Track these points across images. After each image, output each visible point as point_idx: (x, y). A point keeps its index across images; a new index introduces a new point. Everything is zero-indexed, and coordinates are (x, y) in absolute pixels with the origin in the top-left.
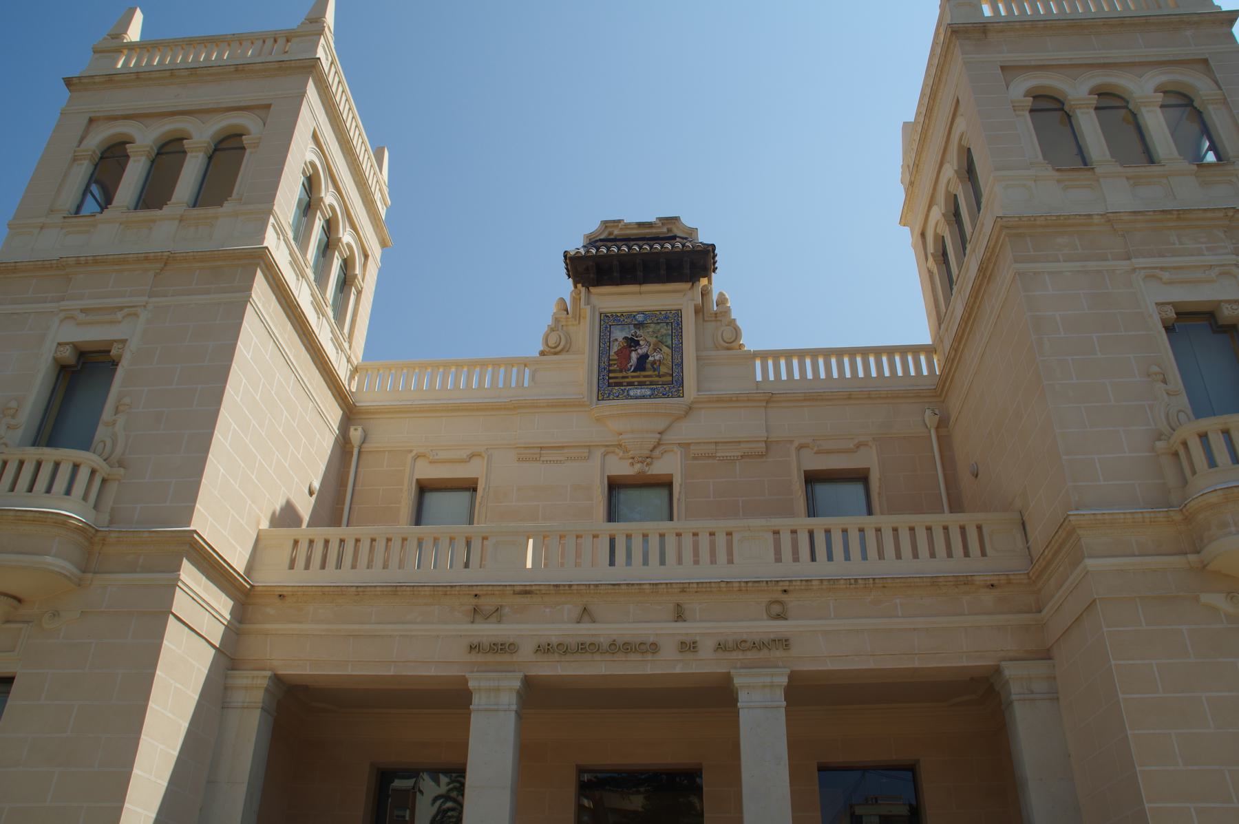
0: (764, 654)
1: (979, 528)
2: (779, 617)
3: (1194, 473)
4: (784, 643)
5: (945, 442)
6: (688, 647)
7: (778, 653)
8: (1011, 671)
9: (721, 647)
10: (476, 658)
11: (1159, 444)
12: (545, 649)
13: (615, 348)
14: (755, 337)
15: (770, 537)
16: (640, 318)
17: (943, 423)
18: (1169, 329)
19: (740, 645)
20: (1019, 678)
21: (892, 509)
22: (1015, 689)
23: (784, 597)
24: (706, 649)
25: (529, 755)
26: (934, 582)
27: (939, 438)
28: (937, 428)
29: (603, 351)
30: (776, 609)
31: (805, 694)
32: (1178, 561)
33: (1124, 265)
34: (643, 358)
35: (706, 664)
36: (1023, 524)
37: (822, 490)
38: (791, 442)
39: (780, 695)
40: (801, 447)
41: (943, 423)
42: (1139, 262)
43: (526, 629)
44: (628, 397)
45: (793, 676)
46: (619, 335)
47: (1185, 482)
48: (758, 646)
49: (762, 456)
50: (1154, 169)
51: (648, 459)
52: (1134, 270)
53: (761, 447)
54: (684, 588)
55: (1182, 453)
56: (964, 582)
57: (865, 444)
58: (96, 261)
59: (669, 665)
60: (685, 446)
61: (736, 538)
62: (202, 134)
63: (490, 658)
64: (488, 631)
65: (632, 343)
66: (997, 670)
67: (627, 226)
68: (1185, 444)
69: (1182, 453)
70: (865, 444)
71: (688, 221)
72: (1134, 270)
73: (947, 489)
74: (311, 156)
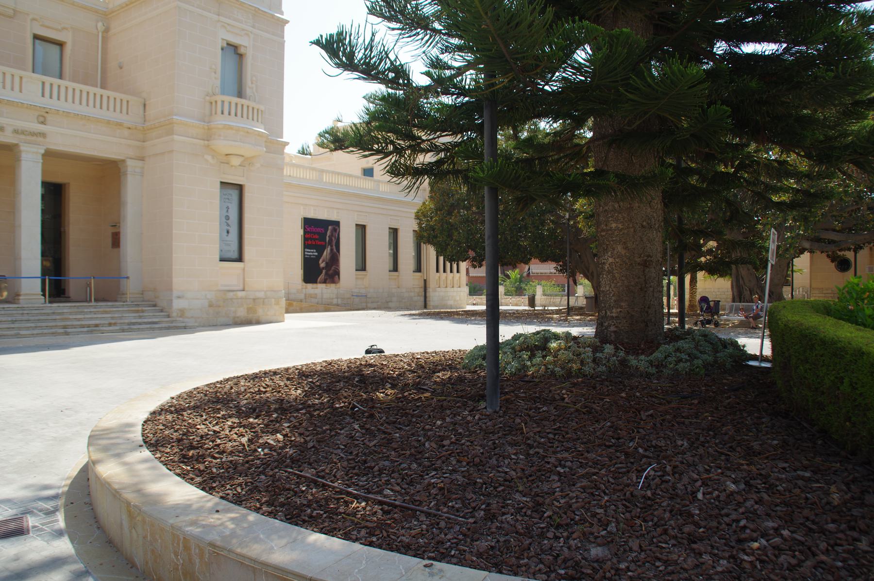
0: (34, 138)
1: (128, 102)
2: (43, 123)
4: (43, 135)
5: (105, 40)
7: (40, 139)
8: (130, 163)
9: (16, 131)
11: (208, 98)
17: (107, 30)
18: (222, 49)
19: (23, 133)
20: (132, 166)
22: (129, 169)
23: (46, 115)
26: (109, 122)
27: (103, 37)
28: (103, 32)
30: (42, 119)
31: (49, 155)
32: (202, 142)
33: (215, 17)
36: (145, 105)
37: (235, 194)
38: (28, 14)
39: (40, 157)
40: (33, 19)
41: (107, 30)
42: (222, 19)
47: (211, 115)
48: (33, 134)
49: (10, 17)
52: (219, 21)
53: (11, 12)
55: (214, 104)
56: (119, 125)
57: (66, 29)
61: (24, 80)
66: (123, 161)
68: (216, 102)
69: (214, 104)
70: (66, 29)
72: (219, 21)
73: (102, 63)
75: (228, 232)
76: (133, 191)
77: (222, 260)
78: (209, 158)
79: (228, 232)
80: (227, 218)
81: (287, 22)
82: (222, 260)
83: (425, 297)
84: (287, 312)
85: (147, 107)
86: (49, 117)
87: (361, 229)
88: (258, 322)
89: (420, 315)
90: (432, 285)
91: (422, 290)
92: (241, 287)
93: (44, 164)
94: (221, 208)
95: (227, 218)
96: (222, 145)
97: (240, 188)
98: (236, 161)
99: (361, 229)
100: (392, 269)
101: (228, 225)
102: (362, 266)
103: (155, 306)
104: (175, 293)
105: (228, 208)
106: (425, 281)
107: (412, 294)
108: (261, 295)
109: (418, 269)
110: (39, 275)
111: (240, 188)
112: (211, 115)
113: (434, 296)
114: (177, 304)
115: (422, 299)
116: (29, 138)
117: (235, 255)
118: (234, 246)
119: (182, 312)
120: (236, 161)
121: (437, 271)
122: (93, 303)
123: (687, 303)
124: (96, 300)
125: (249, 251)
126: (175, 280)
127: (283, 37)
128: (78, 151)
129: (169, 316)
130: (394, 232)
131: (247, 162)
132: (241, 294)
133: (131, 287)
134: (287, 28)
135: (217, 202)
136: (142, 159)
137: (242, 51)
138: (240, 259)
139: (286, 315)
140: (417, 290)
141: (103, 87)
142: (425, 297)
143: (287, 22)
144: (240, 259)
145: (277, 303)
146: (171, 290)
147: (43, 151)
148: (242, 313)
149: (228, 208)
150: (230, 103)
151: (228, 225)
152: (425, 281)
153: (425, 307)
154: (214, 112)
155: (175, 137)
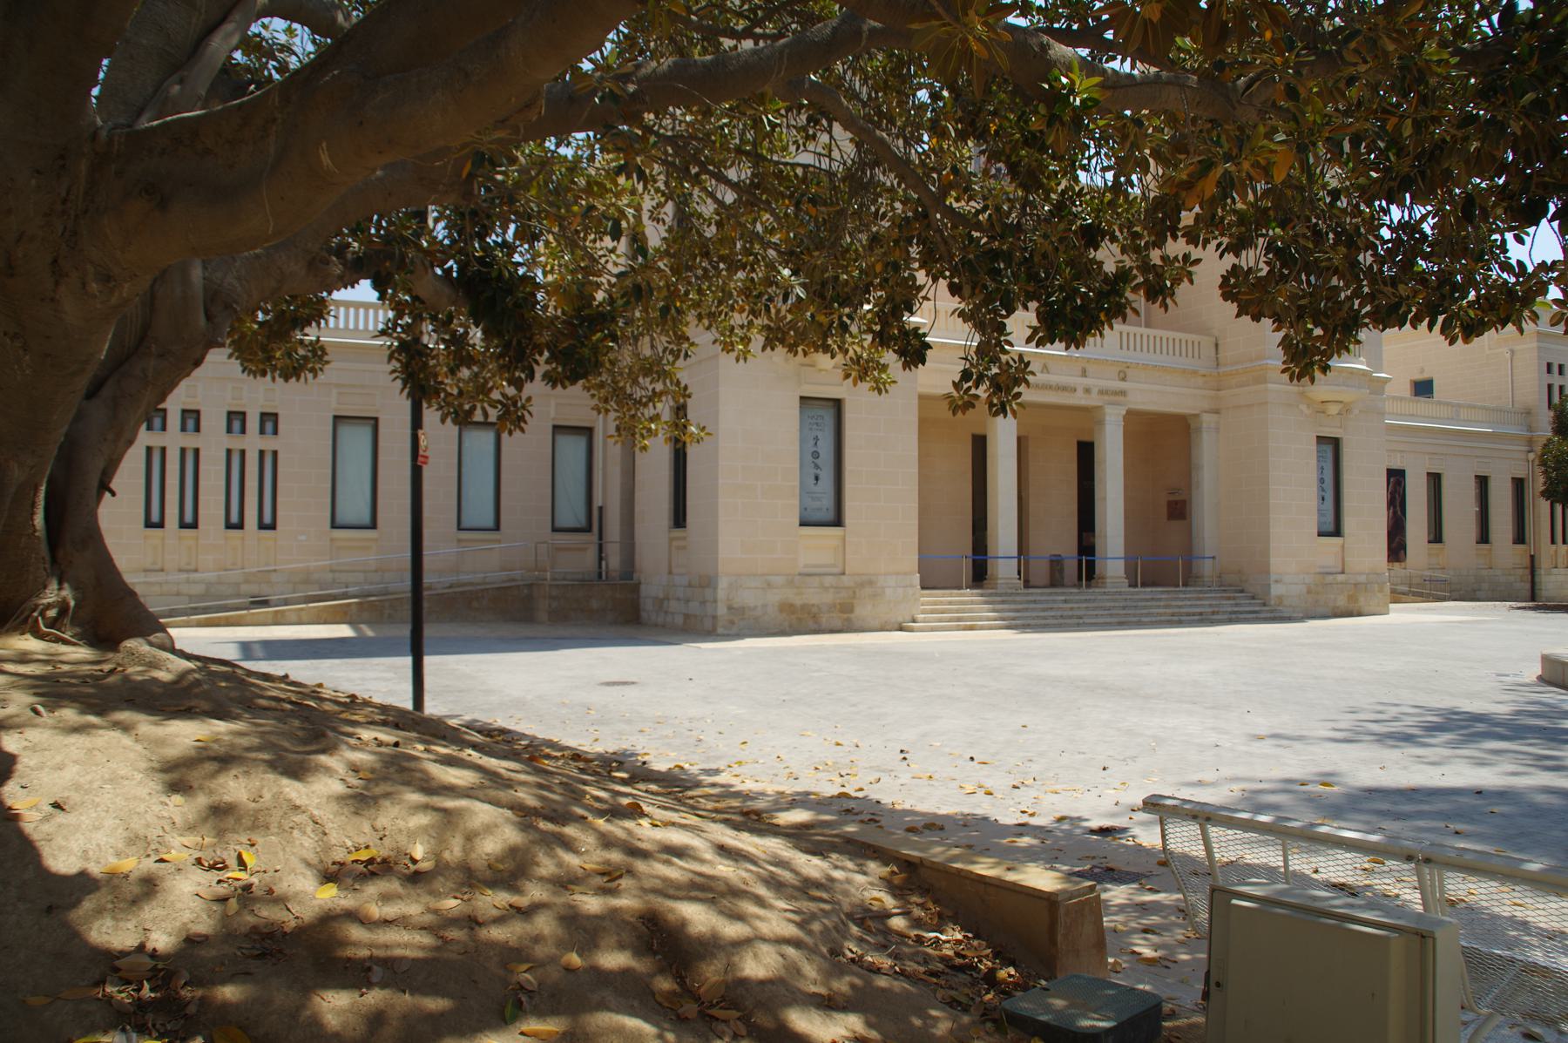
2: (1124, 379)
4: (1123, 393)
6: (1087, 391)
7: (1121, 398)
9: (1101, 392)
20: (1208, 420)
24: (1095, 391)
26: (1184, 371)
37: (1329, 449)
48: (1116, 393)
59: (1079, 399)
66: (1196, 416)
75: (817, 478)
76: (1210, 454)
77: (802, 524)
78: (1303, 407)
79: (817, 478)
80: (816, 455)
82: (1320, 534)
86: (1129, 372)
87: (1435, 480)
88: (1360, 615)
89: (1530, 608)
90: (1544, 563)
91: (1528, 572)
94: (802, 441)
95: (816, 455)
99: (1435, 480)
101: (817, 467)
102: (1436, 536)
103: (1242, 591)
104: (1273, 577)
105: (816, 439)
106: (1532, 557)
107: (1512, 579)
108: (1362, 579)
109: (1520, 538)
114: (1276, 590)
115: (1528, 586)
116: (1112, 398)
117: (830, 516)
118: (828, 502)
119: (1280, 598)
120: (1333, 409)
121: (1553, 542)
123: (344, 631)
124: (1143, 585)
125: (1349, 523)
126: (1272, 560)
130: (1483, 482)
131: (1346, 409)
132: (1340, 578)
133: (1207, 568)
135: (1314, 461)
136: (1217, 412)
138: (838, 522)
139: (1392, 606)
140: (1520, 572)
141: (1148, 325)
144: (838, 522)
145: (1381, 591)
146: (1268, 572)
148: (1342, 602)
149: (816, 439)
151: (817, 467)
152: (1532, 557)
153: (1533, 600)
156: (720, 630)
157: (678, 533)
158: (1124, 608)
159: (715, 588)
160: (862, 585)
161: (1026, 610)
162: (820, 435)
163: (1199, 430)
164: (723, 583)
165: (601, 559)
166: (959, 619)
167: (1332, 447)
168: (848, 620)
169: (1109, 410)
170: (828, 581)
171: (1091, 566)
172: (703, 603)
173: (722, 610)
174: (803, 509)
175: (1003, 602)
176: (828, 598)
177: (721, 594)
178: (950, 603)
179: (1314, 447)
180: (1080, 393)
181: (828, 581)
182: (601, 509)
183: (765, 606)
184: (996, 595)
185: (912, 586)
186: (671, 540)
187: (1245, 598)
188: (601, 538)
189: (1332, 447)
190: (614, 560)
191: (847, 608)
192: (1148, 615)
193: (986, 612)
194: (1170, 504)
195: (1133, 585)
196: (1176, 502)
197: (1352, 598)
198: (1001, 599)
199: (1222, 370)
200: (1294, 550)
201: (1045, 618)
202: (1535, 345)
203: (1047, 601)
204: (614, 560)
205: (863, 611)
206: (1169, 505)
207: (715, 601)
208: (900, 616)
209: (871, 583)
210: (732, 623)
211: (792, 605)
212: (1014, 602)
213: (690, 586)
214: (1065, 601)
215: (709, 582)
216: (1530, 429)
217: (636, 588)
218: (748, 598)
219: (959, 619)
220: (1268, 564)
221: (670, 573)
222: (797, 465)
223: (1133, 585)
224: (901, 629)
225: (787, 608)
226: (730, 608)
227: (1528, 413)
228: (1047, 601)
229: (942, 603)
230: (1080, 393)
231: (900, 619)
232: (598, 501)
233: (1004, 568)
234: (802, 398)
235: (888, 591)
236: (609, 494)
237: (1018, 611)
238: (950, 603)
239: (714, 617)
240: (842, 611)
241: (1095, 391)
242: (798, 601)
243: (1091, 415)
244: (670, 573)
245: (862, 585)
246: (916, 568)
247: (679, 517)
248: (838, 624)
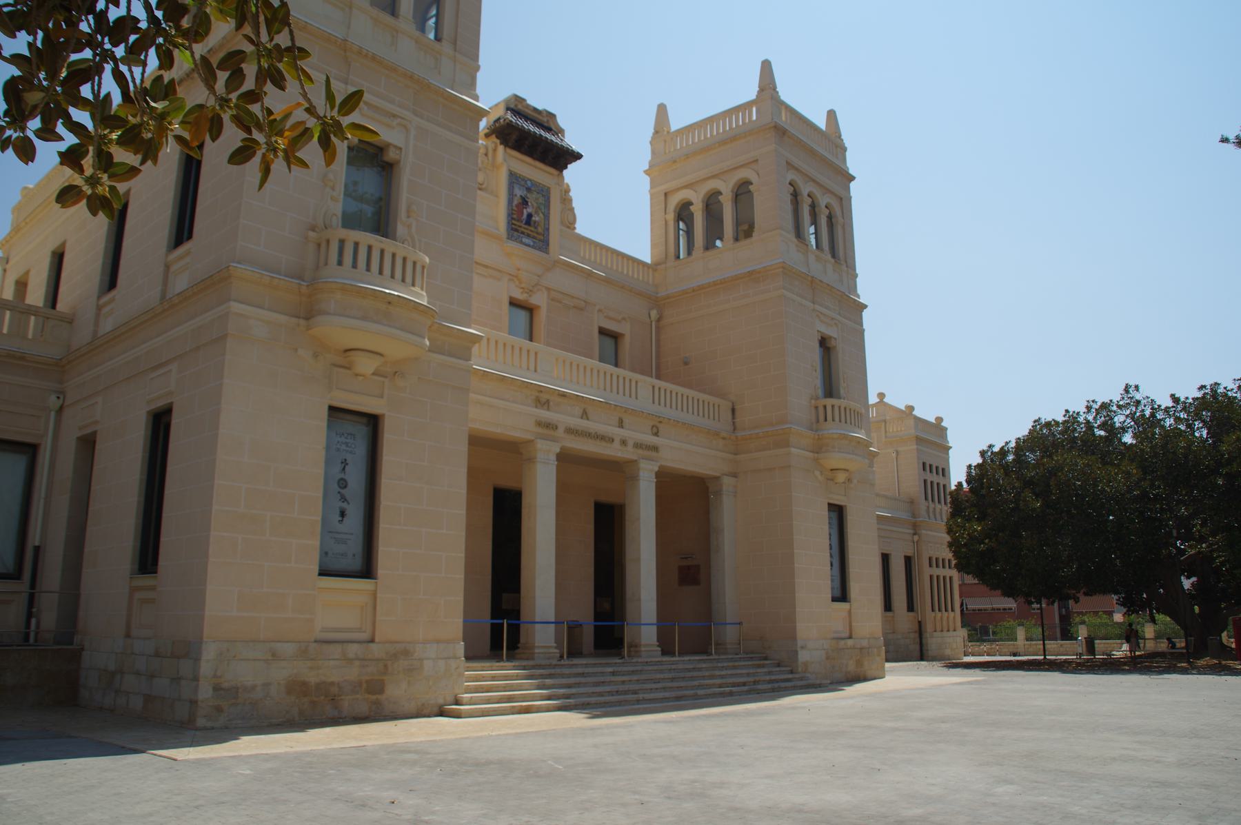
2: (656, 434)
3: (326, 264)
4: (655, 449)
6: (624, 442)
9: (638, 446)
10: (540, 430)
11: (311, 234)
12: (570, 431)
13: (515, 202)
14: (581, 228)
15: (539, 369)
16: (529, 183)
20: (727, 482)
21: (633, 370)
22: (724, 488)
24: (631, 443)
25: (563, 489)
29: (510, 201)
32: (811, 454)
34: (530, 216)
35: (627, 453)
36: (733, 411)
37: (361, 431)
42: (817, 307)
43: (565, 418)
44: (521, 242)
45: (661, 467)
46: (519, 192)
47: (317, 267)
50: (388, 18)
51: (531, 292)
54: (626, 410)
55: (324, 245)
58: (374, 58)
60: (548, 289)
62: (726, 188)
63: (545, 431)
64: (544, 414)
65: (524, 202)
66: (717, 478)
67: (528, 106)
68: (328, 241)
69: (324, 245)
71: (562, 121)
74: (810, 200)
75: (343, 514)
76: (730, 518)
77: (323, 573)
78: (817, 473)
79: (343, 514)
80: (343, 484)
81: (866, 307)
83: (921, 644)
84: (887, 661)
85: (737, 413)
90: (929, 627)
92: (847, 635)
93: (471, 455)
94: (328, 462)
95: (343, 484)
96: (834, 460)
97: (373, 422)
98: (367, 366)
100: (838, 594)
104: (800, 643)
108: (865, 643)
109: (911, 608)
110: (655, 621)
111: (373, 422)
112: (317, 267)
113: (933, 642)
114: (803, 656)
115: (917, 647)
119: (806, 664)
120: (841, 477)
122: (715, 657)
124: (680, 654)
127: (861, 325)
128: (499, 431)
129: (792, 672)
131: (392, 372)
132: (850, 642)
133: (730, 634)
134: (865, 313)
136: (735, 475)
137: (391, 155)
138: (367, 571)
139: (888, 665)
140: (912, 635)
142: (921, 644)
143: (866, 307)
144: (367, 571)
147: (558, 450)
148: (851, 667)
150: (370, 248)
154: (822, 418)
155: (793, 450)
156: (201, 722)
157: (146, 580)
158: (673, 679)
159: (197, 660)
160: (395, 656)
161: (578, 685)
162: (349, 457)
163: (719, 493)
164: (209, 653)
165: (30, 615)
166: (510, 699)
167: (838, 513)
168: (378, 703)
169: (643, 464)
170: (353, 650)
171: (515, 631)
172: (176, 680)
173: (205, 692)
174: (324, 554)
175: (550, 676)
176: (352, 673)
177: (206, 668)
178: (494, 678)
179: (826, 513)
180: (617, 444)
181: (353, 650)
182: (37, 549)
183: (267, 685)
184: (533, 667)
185: (456, 658)
186: (133, 590)
187: (771, 669)
188: (33, 586)
189: (838, 513)
190: (49, 617)
191: (376, 687)
192: (700, 687)
193: (529, 689)
194: (681, 569)
195: (665, 652)
196: (689, 568)
197: (859, 663)
198: (542, 672)
199: (740, 434)
200: (815, 620)
201: (601, 694)
202: (915, 447)
203: (594, 674)
204: (49, 617)
205: (396, 691)
206: (689, 573)
207: (196, 679)
208: (440, 696)
209: (406, 653)
210: (219, 709)
211: (304, 684)
212: (562, 676)
213: (157, 654)
214: (613, 673)
215: (188, 650)
216: (914, 516)
217: (76, 656)
218: (244, 673)
219: (510, 699)
220: (793, 630)
221: (128, 636)
222: (320, 494)
223: (665, 652)
224: (442, 713)
225: (297, 688)
226: (217, 688)
227: (912, 502)
228: (594, 674)
229: (483, 678)
230: (617, 444)
231: (441, 701)
232: (34, 538)
233: (543, 636)
234: (333, 410)
235: (428, 665)
236: (50, 529)
237: (569, 686)
238: (494, 678)
239: (194, 702)
240: (370, 691)
241: (631, 443)
242: (312, 678)
243: (622, 470)
244: (128, 636)
245: (395, 656)
246: (460, 633)
247: (148, 557)
248: (363, 709)
